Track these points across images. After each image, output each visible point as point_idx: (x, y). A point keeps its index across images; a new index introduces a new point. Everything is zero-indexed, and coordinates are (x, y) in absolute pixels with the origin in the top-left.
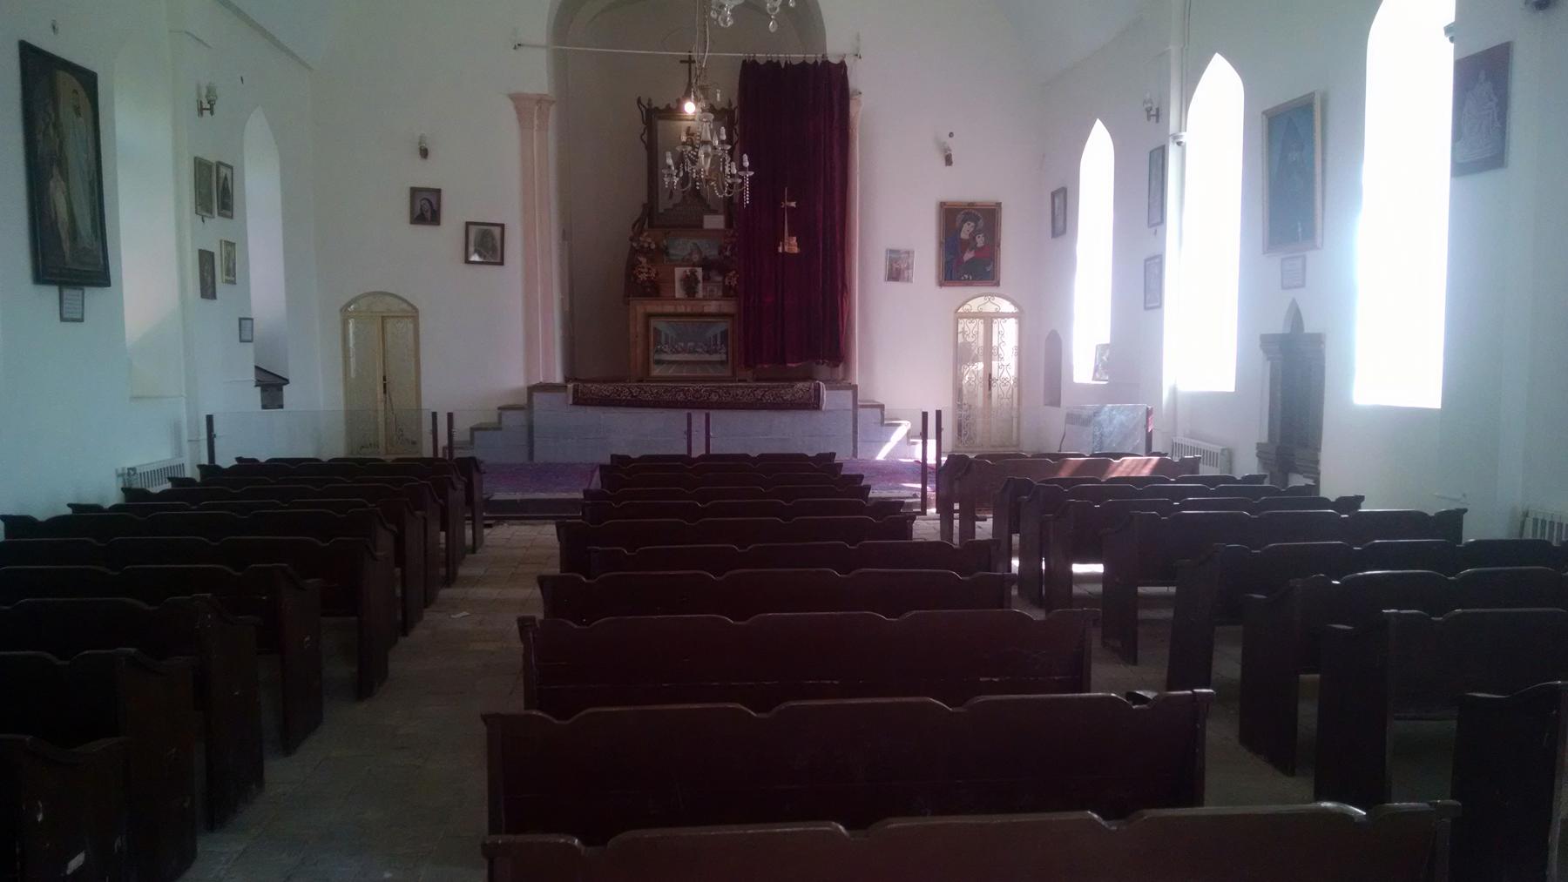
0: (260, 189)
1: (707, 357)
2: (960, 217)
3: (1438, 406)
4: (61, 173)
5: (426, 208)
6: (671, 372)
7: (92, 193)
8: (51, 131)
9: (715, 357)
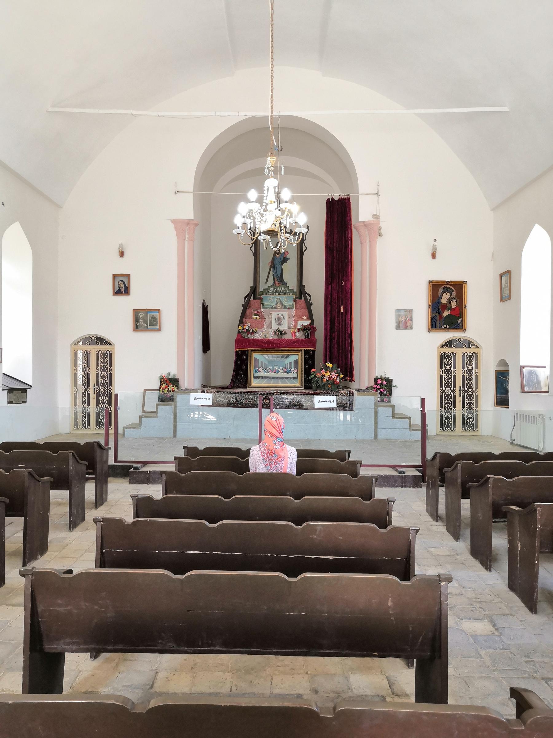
1: (286, 375)
2: (441, 290)
3: (536, 224)
5: (122, 287)
6: (264, 383)
9: (291, 375)
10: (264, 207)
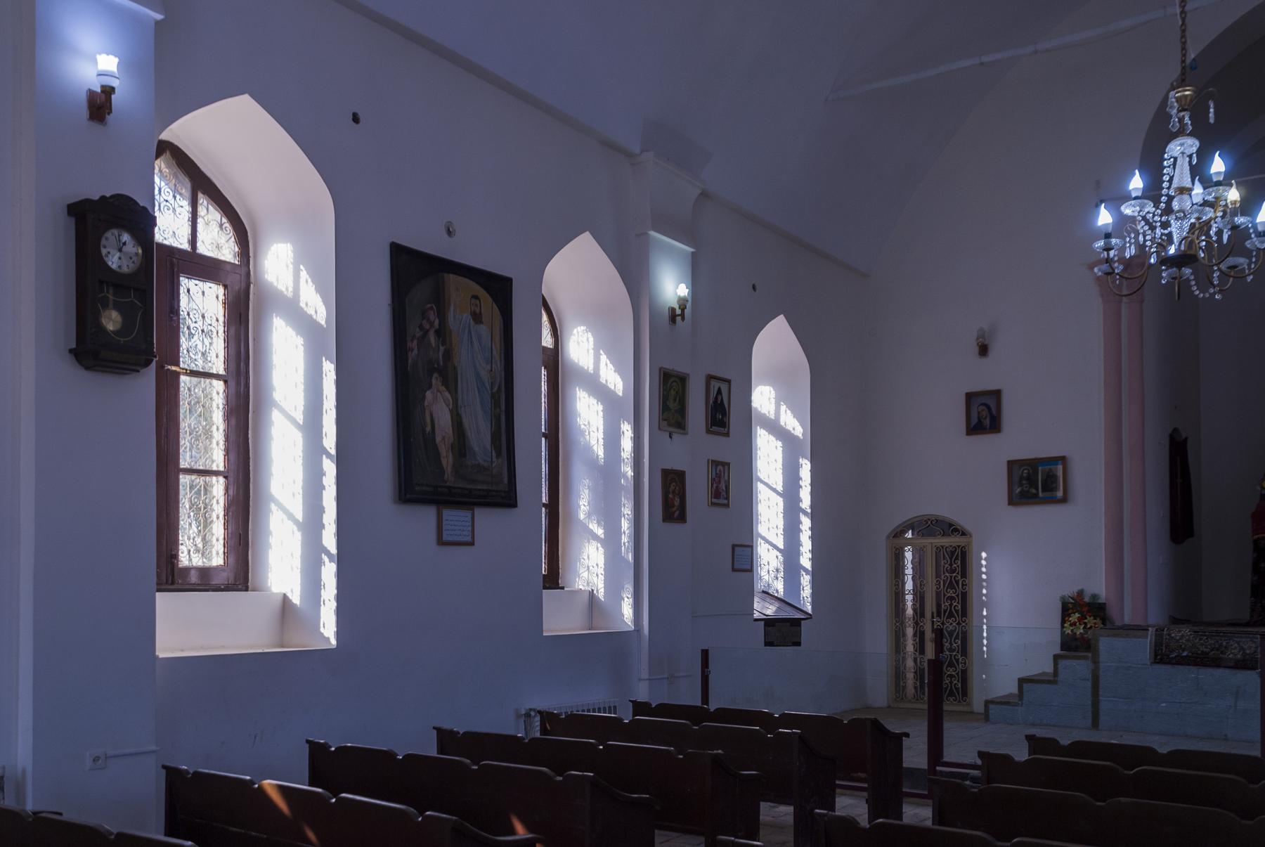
0: (776, 407)
3: (782, 317)
4: (445, 383)
5: (984, 414)
7: (496, 404)
8: (432, 338)
10: (1163, 205)
